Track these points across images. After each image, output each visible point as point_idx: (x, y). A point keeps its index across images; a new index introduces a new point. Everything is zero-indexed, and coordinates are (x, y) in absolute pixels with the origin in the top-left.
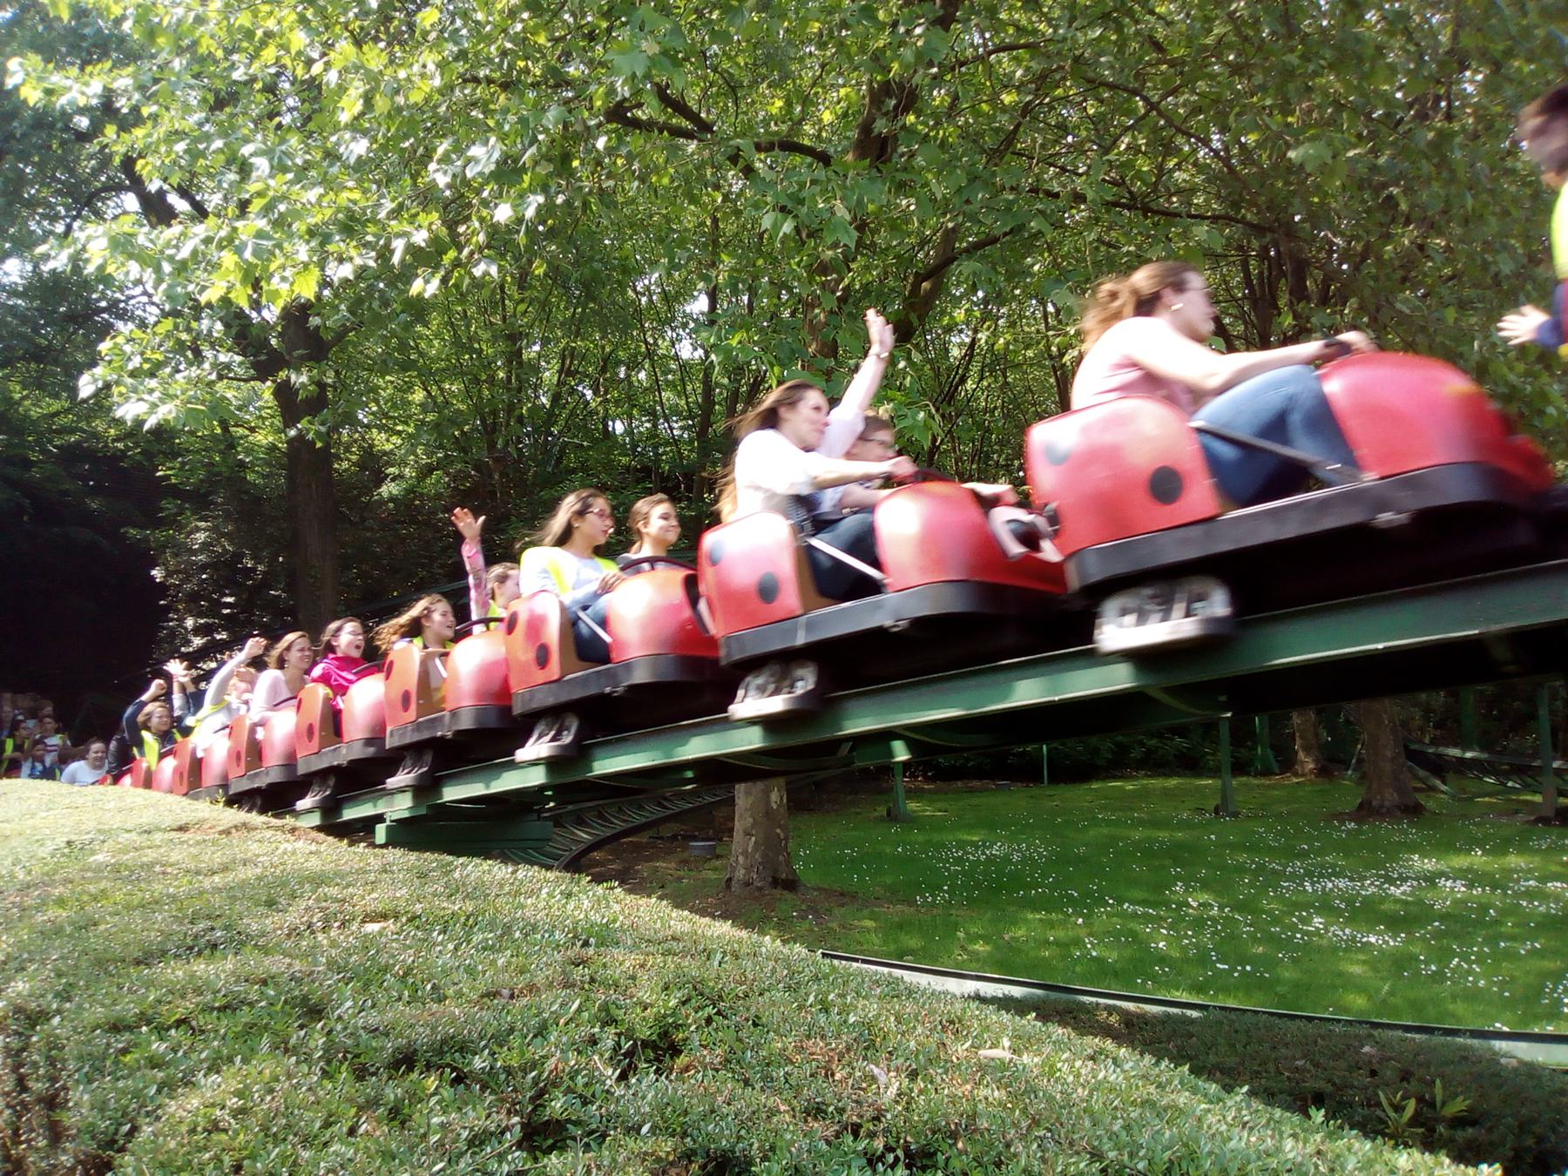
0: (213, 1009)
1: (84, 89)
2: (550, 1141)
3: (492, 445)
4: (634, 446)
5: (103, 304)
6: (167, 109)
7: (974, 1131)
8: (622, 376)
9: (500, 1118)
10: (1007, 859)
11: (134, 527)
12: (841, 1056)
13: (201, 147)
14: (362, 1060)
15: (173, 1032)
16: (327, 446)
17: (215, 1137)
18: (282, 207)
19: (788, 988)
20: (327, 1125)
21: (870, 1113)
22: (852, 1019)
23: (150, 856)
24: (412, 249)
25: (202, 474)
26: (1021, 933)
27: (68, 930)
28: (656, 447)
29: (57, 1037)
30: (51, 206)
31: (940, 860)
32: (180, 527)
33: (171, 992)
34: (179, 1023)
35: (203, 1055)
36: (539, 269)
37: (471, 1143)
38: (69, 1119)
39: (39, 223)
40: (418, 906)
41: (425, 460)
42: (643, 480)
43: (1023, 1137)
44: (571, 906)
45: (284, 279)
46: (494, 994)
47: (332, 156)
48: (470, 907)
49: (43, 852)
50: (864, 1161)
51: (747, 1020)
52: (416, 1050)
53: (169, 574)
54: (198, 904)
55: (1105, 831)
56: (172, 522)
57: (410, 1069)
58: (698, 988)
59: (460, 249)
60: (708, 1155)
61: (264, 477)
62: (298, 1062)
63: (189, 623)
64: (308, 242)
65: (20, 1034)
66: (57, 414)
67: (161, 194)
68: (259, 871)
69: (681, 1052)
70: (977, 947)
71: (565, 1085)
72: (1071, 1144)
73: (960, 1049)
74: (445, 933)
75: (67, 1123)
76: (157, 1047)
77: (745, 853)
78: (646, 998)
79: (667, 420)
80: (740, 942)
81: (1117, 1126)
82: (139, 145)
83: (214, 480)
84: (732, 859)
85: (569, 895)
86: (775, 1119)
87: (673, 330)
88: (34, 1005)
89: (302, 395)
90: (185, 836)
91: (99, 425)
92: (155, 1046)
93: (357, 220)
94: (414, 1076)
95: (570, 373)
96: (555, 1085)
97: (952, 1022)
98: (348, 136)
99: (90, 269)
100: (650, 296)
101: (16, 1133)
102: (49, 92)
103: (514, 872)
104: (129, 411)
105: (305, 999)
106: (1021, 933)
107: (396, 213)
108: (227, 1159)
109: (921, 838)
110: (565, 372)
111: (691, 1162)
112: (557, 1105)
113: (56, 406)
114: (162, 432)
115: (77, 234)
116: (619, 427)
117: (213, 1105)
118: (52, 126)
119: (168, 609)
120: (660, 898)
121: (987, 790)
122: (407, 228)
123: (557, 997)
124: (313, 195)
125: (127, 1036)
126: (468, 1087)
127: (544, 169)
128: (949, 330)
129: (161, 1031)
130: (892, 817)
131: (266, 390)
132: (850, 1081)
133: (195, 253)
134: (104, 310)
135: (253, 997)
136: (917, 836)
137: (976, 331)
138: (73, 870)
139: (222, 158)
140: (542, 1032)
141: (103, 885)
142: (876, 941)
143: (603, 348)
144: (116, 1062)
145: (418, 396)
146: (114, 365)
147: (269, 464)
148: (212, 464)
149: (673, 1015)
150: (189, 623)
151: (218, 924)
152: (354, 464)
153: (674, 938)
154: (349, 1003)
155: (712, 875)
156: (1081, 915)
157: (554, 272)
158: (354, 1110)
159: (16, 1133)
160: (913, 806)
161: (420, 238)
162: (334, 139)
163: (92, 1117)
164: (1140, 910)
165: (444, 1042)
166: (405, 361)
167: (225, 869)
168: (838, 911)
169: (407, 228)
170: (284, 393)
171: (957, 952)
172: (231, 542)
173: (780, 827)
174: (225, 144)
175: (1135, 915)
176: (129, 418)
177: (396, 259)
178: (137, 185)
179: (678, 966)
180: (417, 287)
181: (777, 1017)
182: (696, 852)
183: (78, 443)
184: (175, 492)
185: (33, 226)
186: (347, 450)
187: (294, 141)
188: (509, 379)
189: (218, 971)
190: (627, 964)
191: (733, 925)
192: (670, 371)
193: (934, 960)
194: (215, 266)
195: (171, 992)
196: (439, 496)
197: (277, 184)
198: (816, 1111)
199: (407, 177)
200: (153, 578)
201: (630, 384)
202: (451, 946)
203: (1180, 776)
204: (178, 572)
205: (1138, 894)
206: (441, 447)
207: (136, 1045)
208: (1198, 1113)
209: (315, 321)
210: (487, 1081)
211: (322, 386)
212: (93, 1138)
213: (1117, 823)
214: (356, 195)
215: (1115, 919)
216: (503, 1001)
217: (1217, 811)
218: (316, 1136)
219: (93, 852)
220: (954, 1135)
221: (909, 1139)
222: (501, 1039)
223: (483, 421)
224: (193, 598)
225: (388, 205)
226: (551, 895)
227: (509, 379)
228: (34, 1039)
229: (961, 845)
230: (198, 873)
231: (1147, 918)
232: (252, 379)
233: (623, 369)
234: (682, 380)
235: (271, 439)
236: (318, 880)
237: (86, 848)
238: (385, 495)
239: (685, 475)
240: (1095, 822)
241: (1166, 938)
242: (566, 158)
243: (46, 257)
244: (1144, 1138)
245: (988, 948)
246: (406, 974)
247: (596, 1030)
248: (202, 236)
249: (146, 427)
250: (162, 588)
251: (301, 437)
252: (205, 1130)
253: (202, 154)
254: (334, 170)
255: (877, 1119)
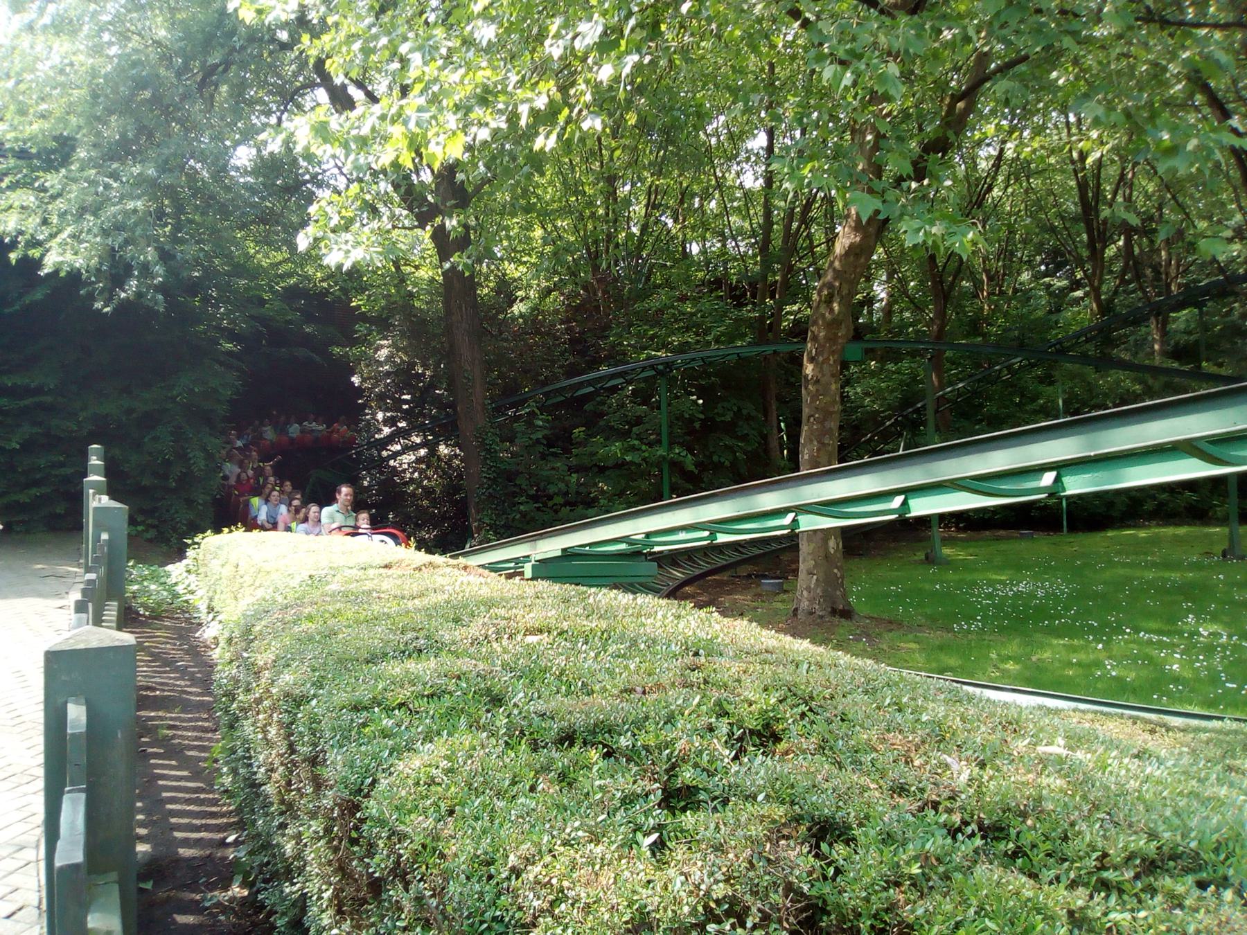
0: (423, 696)
1: (285, 7)
2: (682, 804)
3: (596, 268)
4: (708, 263)
5: (307, 177)
6: (345, 17)
7: (1041, 812)
8: (696, 205)
9: (644, 784)
10: (1032, 595)
11: (337, 346)
12: (917, 748)
13: (372, 45)
14: (535, 736)
15: (397, 712)
16: (472, 276)
17: (433, 788)
18: (436, 88)
19: (866, 692)
20: (514, 783)
21: (946, 794)
22: (924, 718)
23: (369, 585)
24: (534, 113)
25: (383, 303)
26: (1047, 655)
27: (318, 638)
28: (725, 262)
29: (316, 714)
30: (265, 104)
31: (973, 595)
32: (370, 345)
33: (392, 683)
34: (401, 705)
35: (420, 730)
36: (632, 119)
37: (623, 801)
38: (327, 773)
39: (258, 117)
40: (565, 623)
41: (544, 284)
42: (716, 289)
43: (1086, 818)
44: (681, 626)
45: (438, 144)
46: (632, 691)
47: (468, 42)
48: (604, 624)
49: (294, 583)
50: (945, 831)
51: (836, 716)
52: (575, 731)
53: (364, 380)
54: (406, 620)
55: (1121, 571)
56: (364, 341)
57: (571, 745)
58: (791, 690)
59: (571, 107)
60: (813, 819)
61: (427, 303)
62: (488, 738)
63: (380, 416)
64: (455, 113)
65: (290, 712)
66: (280, 263)
67: (344, 87)
68: (446, 596)
69: (781, 740)
70: (1007, 666)
71: (692, 761)
72: (1130, 826)
73: (1021, 745)
74: (587, 643)
75: (326, 776)
76: (387, 723)
77: (808, 589)
78: (751, 696)
79: (734, 239)
80: (821, 655)
81: (1168, 812)
82: (327, 48)
83: (391, 309)
84: (798, 593)
85: (679, 617)
86: (866, 795)
87: (738, 164)
88: (297, 691)
89: (453, 235)
90: (390, 572)
91: (310, 270)
92: (384, 722)
93: (490, 92)
94: (576, 749)
95: (655, 207)
96: (684, 761)
97: (1010, 723)
98: (480, 22)
99: (299, 149)
100: (719, 137)
101: (289, 783)
102: (260, 12)
103: (635, 599)
104: (333, 258)
105: (489, 690)
106: (1047, 655)
107: (521, 83)
108: (442, 805)
109: (956, 577)
110: (652, 206)
111: (800, 824)
112: (687, 775)
113: (279, 257)
114: (355, 273)
115: (285, 124)
116: (695, 249)
117: (430, 766)
118: (261, 39)
119: (364, 406)
120: (750, 621)
121: (1012, 538)
122: (529, 94)
123: (680, 694)
124: (456, 77)
125: (365, 714)
126: (617, 759)
127: (640, 35)
128: (979, 144)
129: (389, 710)
130: (930, 560)
131: (426, 235)
132: (928, 767)
133: (373, 129)
134: (308, 182)
135: (452, 688)
136: (950, 575)
137: (1004, 142)
138: (316, 595)
139: (387, 53)
140: (670, 720)
141: (338, 606)
142: (920, 659)
143: (681, 183)
144: (359, 733)
145: (538, 233)
146: (321, 223)
147: (429, 293)
148: (389, 296)
149: (773, 710)
150: (380, 416)
151: (421, 634)
152: (492, 290)
153: (767, 651)
154: (521, 695)
155: (779, 605)
156: (1101, 641)
157: (644, 124)
158: (533, 773)
159: (289, 783)
160: (947, 551)
161: (541, 103)
162: (469, 28)
163: (346, 772)
164: (1155, 638)
165: (596, 725)
166: (527, 206)
167: (421, 595)
168: (888, 636)
169: (529, 94)
170: (440, 236)
171: (990, 670)
172: (406, 353)
173: (837, 568)
174: (390, 41)
175: (1150, 642)
176: (333, 265)
177: (523, 123)
178: (326, 80)
179: (774, 673)
180: (539, 143)
181: (861, 715)
182: (768, 588)
183: (296, 285)
184: (364, 318)
185: (255, 121)
186: (486, 279)
187: (439, 32)
188: (607, 214)
189: (425, 668)
190: (733, 670)
191: (812, 642)
192: (736, 199)
193: (971, 676)
194: (386, 138)
195: (392, 683)
196: (556, 312)
197: (431, 70)
198: (901, 790)
199: (527, 53)
200: (353, 383)
201: (704, 213)
202: (592, 654)
203: (1189, 525)
204: (370, 378)
205: (1153, 625)
206: (556, 272)
207: (372, 721)
208: (1239, 803)
209: (460, 177)
210: (632, 756)
211: (466, 227)
212: (346, 787)
213: (1132, 565)
214: (488, 73)
215: (1132, 646)
216: (638, 696)
217: (1224, 554)
218: (506, 791)
219: (328, 583)
220: (1024, 815)
221: (982, 815)
222: (639, 724)
223: (588, 250)
224: (381, 397)
225: (514, 78)
226: (664, 617)
227: (607, 214)
228: (300, 715)
229: (991, 583)
230: (403, 598)
231: (1161, 645)
232: (416, 227)
233: (697, 200)
234: (746, 205)
235: (430, 273)
236: (490, 604)
237: (323, 580)
238: (516, 313)
239: (750, 284)
240: (1111, 564)
241: (1180, 661)
242: (656, 25)
243: (265, 143)
244: (1194, 822)
245: (1017, 667)
246: (561, 674)
247: (713, 720)
248: (378, 114)
249: (344, 269)
250: (359, 391)
251: (453, 268)
252: (425, 783)
253: (374, 51)
254: (471, 54)
255: (952, 798)
